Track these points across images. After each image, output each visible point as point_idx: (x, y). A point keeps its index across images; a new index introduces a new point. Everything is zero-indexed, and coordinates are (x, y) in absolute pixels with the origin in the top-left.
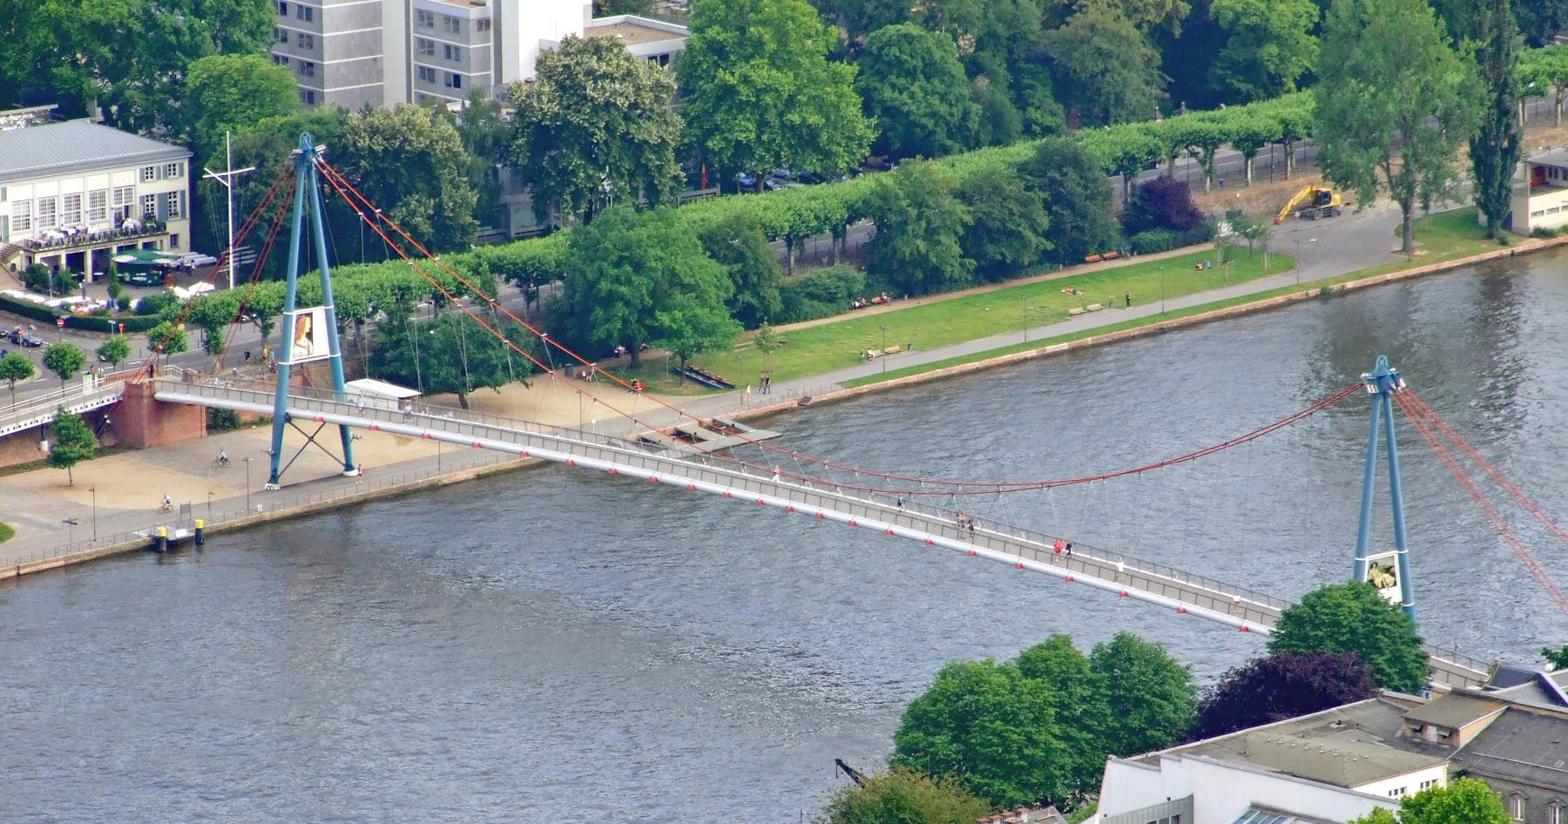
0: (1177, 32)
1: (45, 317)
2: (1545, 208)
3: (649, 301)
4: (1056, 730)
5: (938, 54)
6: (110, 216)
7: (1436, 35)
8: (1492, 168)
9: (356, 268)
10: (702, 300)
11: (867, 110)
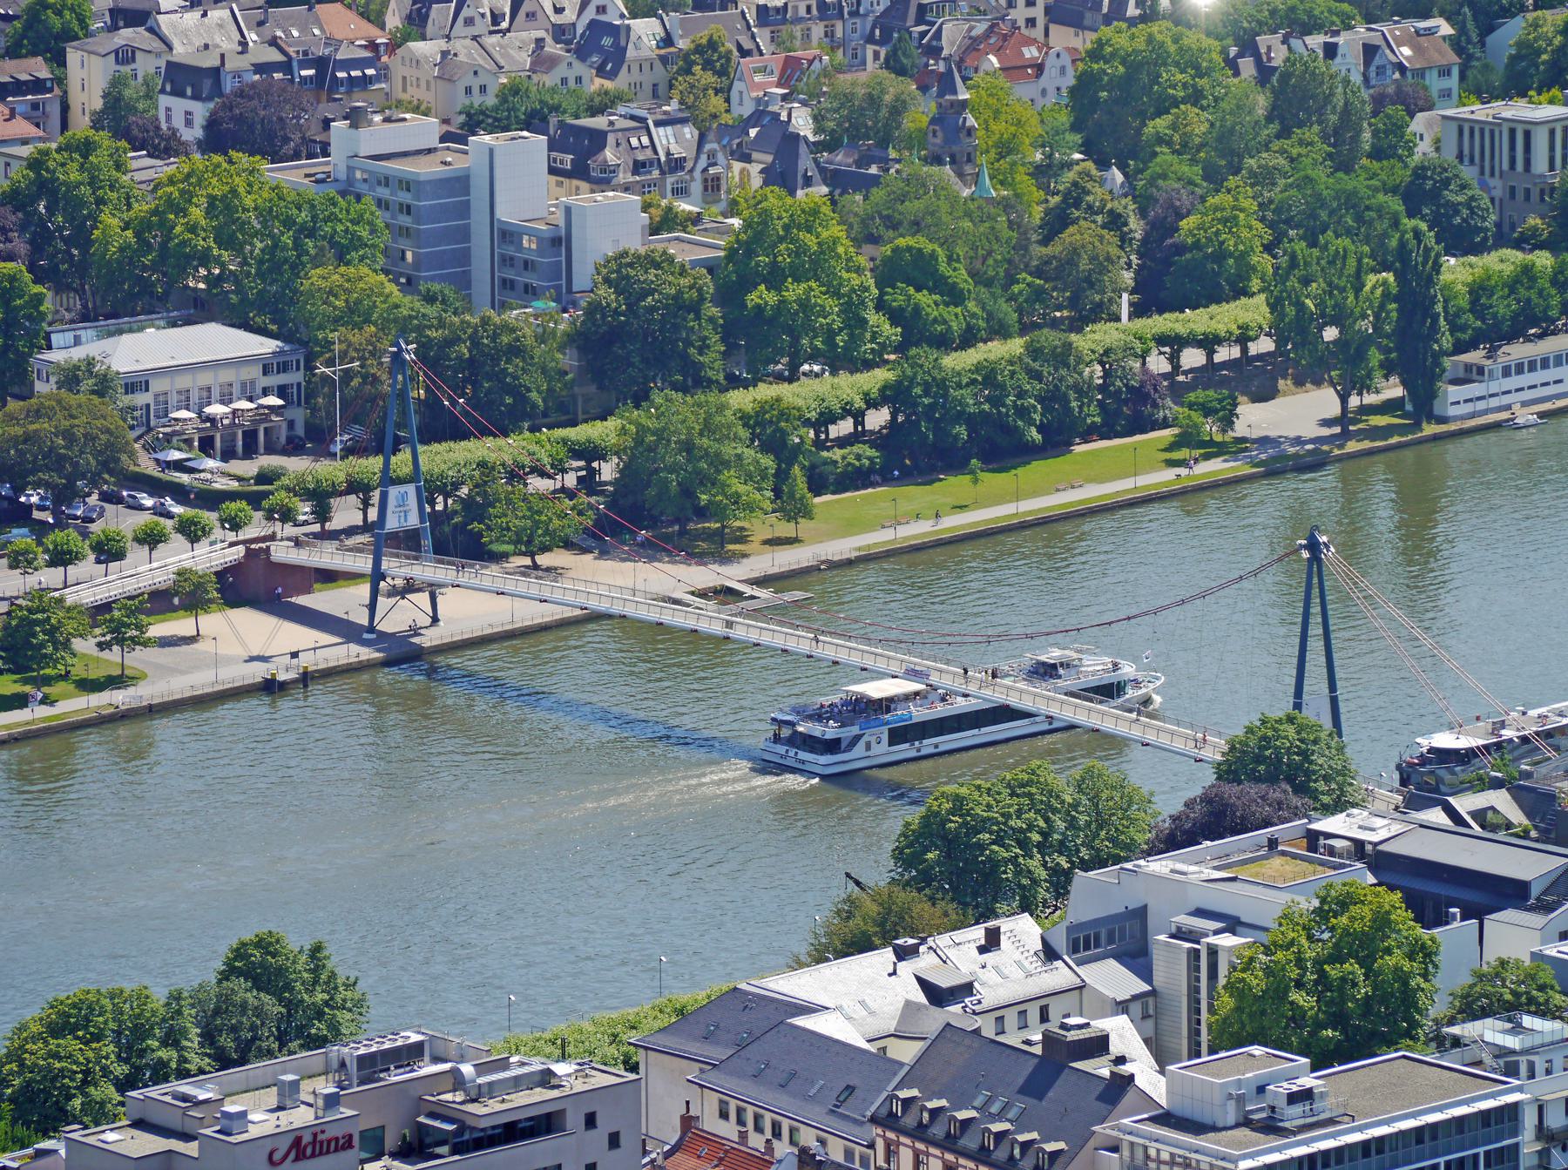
2: (1513, 388)
9: (444, 446)
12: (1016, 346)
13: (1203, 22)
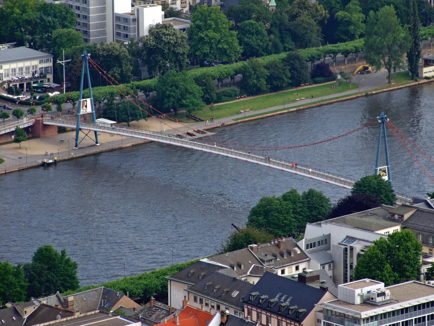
0: (326, 22)
1: (13, 101)
2: (428, 71)
3: (180, 97)
4: (293, 215)
5: (260, 28)
6: (31, 73)
11: (240, 44)
12: (283, 55)
13: (50, 97)
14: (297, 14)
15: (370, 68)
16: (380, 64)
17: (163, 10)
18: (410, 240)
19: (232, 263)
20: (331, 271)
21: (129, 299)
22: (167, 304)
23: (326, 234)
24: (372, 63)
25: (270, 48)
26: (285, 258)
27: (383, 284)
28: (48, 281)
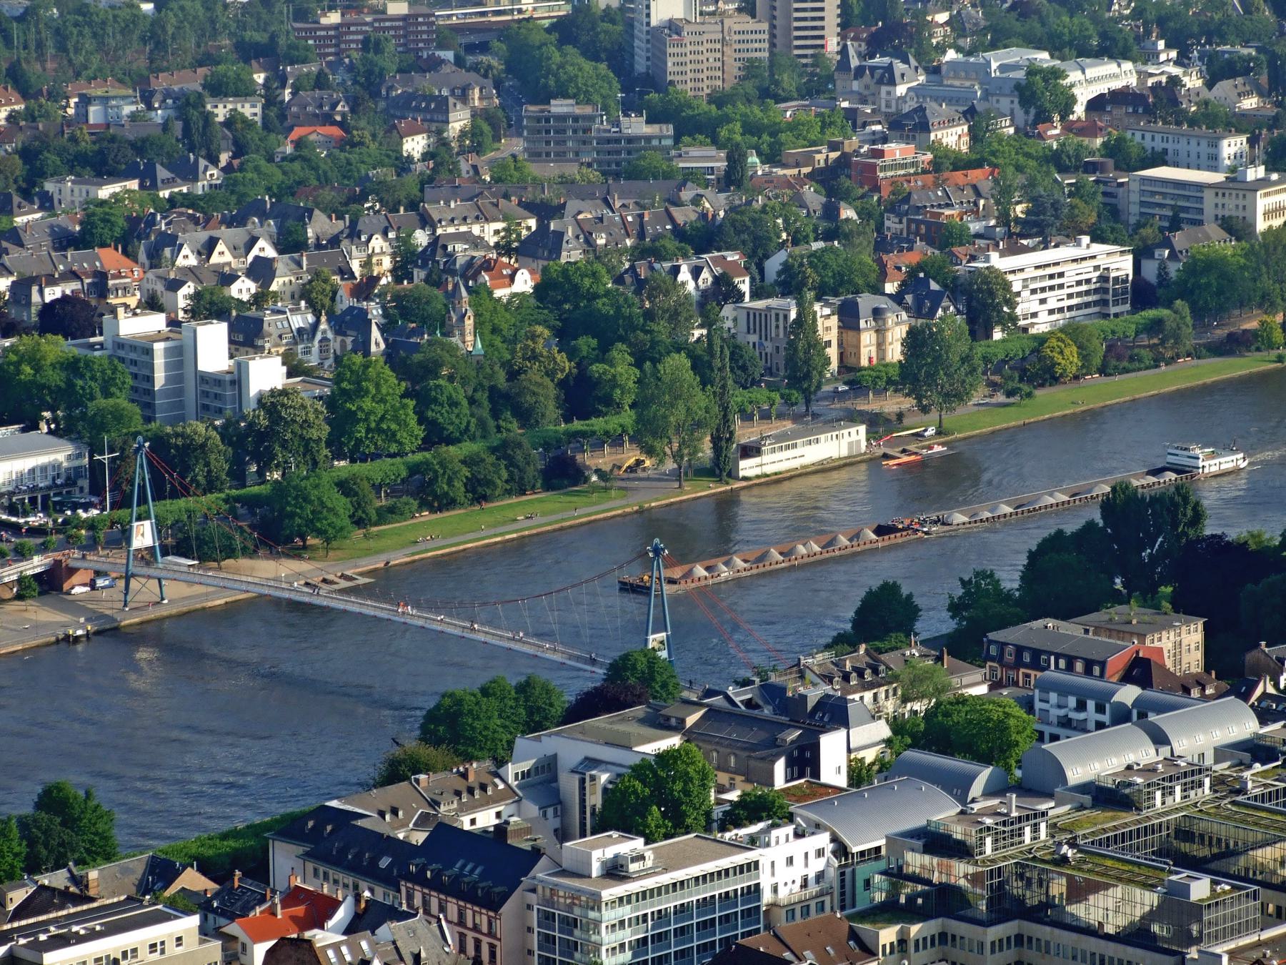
0: (572, 383)
1: (15, 529)
3: (311, 516)
4: (498, 722)
5: (454, 395)
6: (50, 478)
7: (695, 384)
8: (721, 448)
10: (336, 514)
11: (420, 422)
14: (520, 369)
15: (648, 463)
16: (665, 454)
17: (284, 364)
18: (693, 763)
19: (383, 808)
20: (558, 820)
21: (198, 875)
22: (268, 884)
23: (549, 753)
24: (650, 452)
25: (472, 428)
26: (477, 797)
27: (641, 841)
28: (62, 844)
